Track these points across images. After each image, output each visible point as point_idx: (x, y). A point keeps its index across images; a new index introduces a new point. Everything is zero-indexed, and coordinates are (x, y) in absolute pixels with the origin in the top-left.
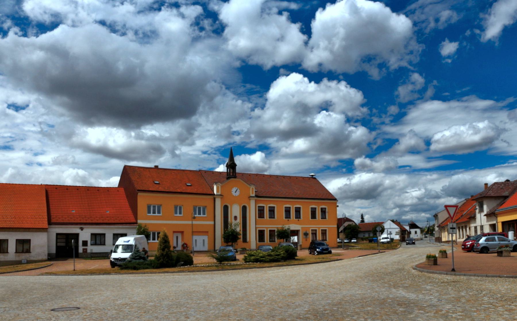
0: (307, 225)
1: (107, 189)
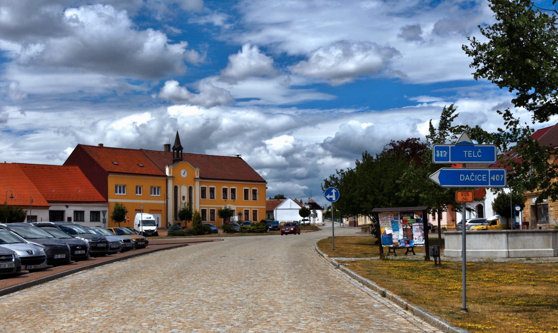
0: (241, 205)
1: (23, 165)
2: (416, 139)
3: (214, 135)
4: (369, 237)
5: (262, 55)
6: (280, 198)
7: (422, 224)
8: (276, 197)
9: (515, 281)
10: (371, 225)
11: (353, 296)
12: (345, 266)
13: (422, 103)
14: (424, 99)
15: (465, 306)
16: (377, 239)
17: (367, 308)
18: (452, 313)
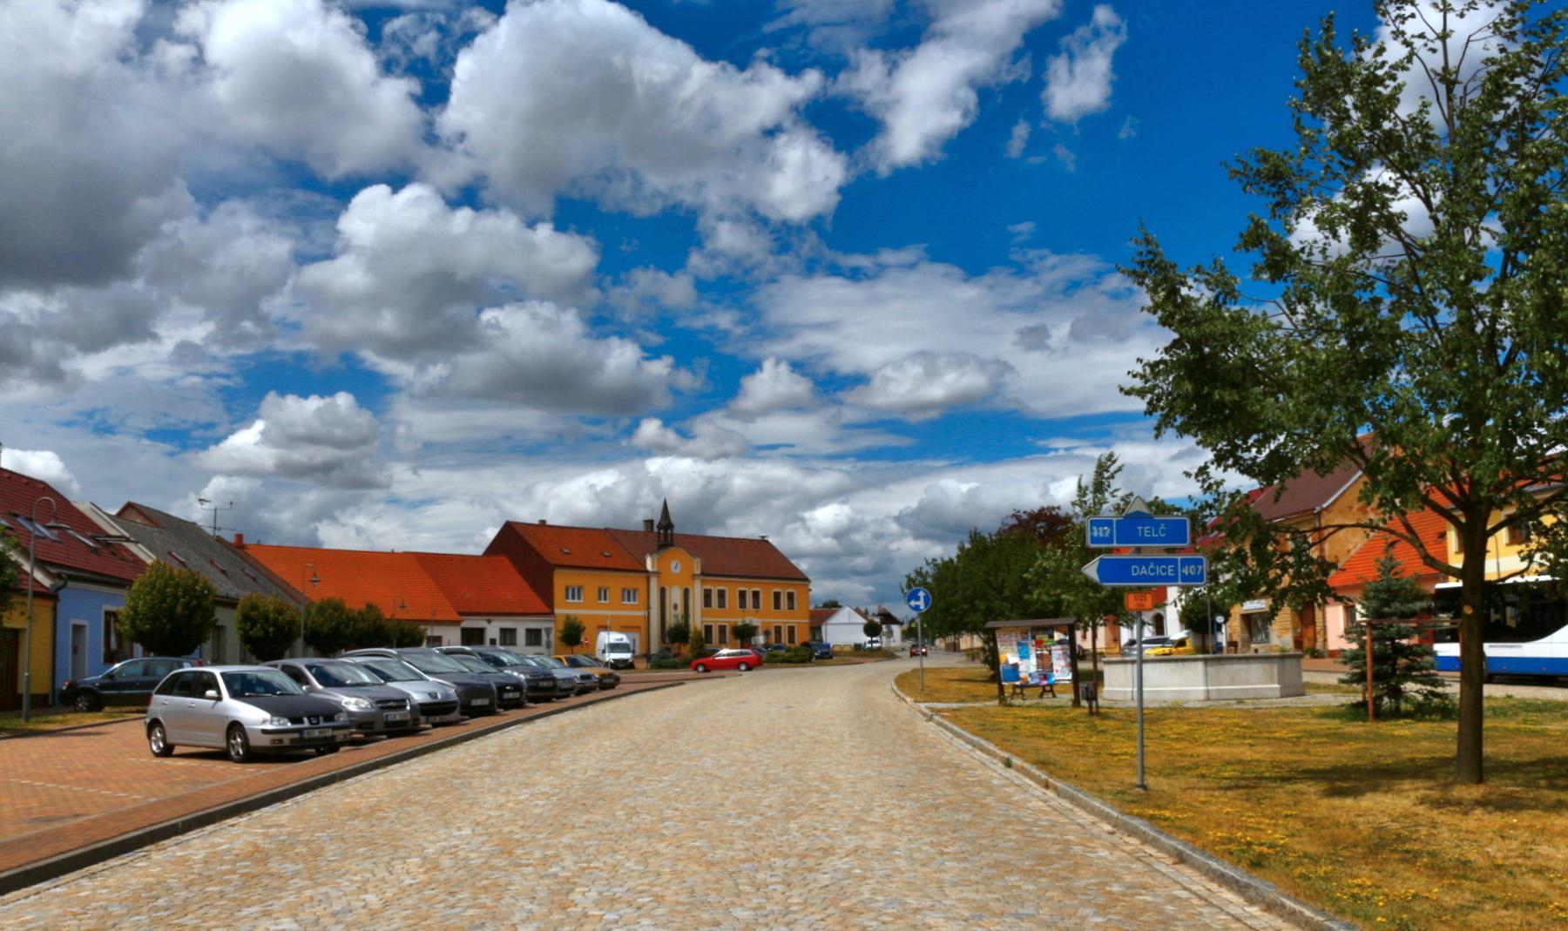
2: (1053, 508)
3: (722, 504)
4: (980, 668)
5: (796, 376)
6: (832, 607)
7: (1067, 647)
8: (826, 605)
9: (1220, 738)
10: (983, 649)
11: (957, 767)
12: (943, 717)
13: (1056, 450)
14: (1060, 443)
15: (1143, 780)
16: (992, 673)
17: (981, 785)
18: (1123, 793)
